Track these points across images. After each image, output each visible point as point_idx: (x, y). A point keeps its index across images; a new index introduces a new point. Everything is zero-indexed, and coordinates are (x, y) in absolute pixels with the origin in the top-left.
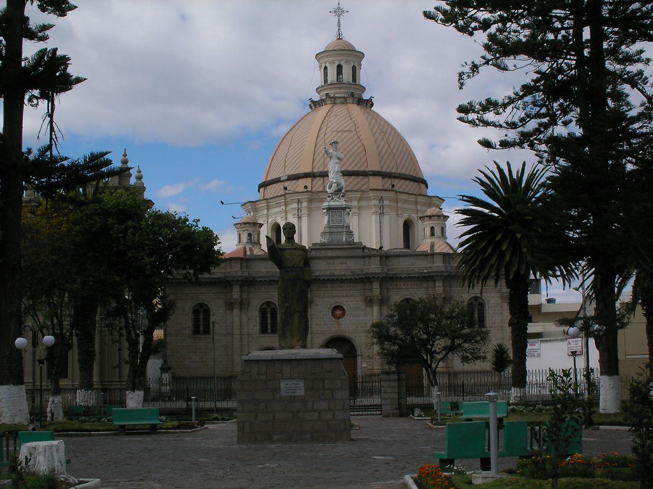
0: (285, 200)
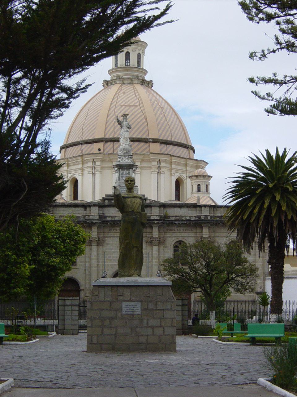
0: (82, 159)
